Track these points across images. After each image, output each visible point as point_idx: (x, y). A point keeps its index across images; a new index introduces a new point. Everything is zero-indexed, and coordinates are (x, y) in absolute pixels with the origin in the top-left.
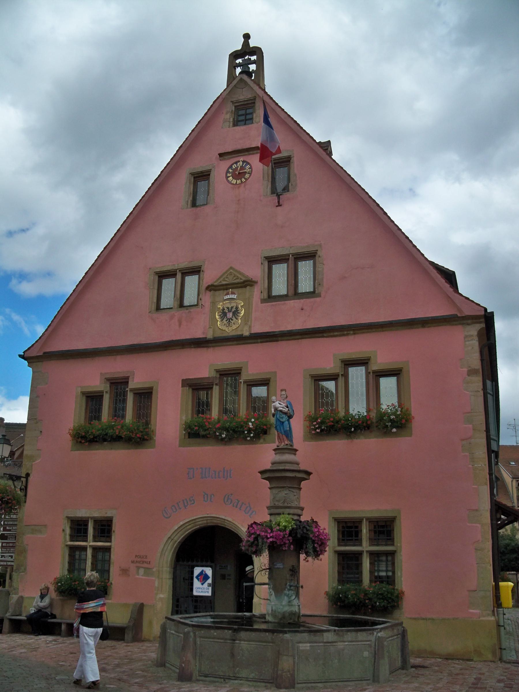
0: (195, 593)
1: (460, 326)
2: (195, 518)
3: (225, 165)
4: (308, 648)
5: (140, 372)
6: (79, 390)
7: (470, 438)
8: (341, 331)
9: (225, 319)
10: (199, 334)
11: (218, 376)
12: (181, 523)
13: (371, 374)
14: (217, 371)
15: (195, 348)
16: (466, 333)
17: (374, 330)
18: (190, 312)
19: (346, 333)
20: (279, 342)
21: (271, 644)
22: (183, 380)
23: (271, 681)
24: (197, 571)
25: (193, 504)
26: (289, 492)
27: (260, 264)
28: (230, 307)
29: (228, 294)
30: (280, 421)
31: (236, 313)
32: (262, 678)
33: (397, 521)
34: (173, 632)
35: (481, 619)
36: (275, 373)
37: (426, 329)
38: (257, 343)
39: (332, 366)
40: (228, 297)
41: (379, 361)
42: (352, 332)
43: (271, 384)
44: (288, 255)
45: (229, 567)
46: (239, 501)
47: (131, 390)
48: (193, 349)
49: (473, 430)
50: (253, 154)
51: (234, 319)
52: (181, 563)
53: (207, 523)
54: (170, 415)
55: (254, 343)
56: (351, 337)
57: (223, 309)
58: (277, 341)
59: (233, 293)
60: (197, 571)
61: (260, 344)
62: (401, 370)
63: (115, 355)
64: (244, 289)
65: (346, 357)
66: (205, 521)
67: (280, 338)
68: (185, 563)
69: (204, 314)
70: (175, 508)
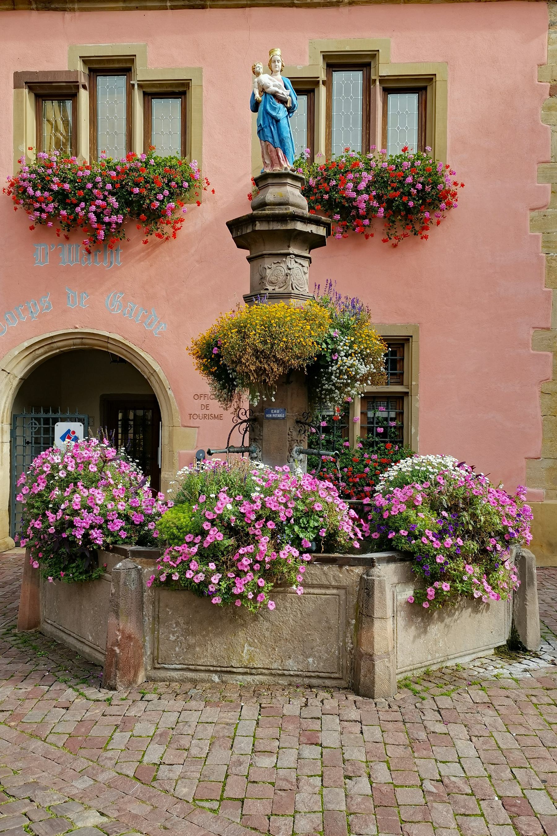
2: (51, 335)
13: (378, 83)
15: (38, 9)
22: (16, 74)
24: (61, 428)
33: (414, 344)
38: (165, 8)
39: (307, 62)
43: (194, 93)
48: (35, 14)
61: (170, 11)
66: (78, 341)
68: (33, 415)
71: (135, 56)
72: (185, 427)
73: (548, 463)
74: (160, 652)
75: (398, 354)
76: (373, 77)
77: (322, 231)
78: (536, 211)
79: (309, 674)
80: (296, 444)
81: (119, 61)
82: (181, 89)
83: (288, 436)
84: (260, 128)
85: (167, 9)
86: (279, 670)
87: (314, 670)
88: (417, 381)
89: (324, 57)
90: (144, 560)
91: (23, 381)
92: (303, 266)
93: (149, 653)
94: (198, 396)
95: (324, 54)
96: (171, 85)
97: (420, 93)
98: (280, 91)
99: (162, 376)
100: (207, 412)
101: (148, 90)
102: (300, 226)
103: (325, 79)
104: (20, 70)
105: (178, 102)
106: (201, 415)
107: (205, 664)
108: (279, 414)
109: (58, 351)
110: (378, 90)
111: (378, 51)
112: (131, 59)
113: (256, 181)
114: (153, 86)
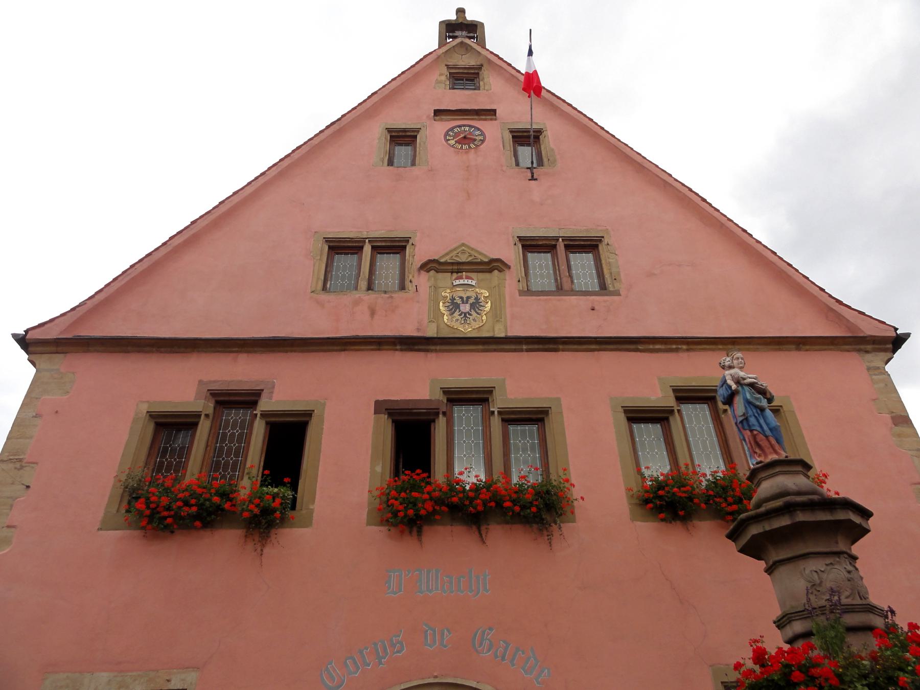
1: (855, 354)
3: (442, 126)
5: (286, 386)
6: (144, 408)
9: (457, 313)
10: (409, 331)
15: (401, 350)
18: (392, 297)
19: (674, 347)
25: (398, 652)
27: (513, 245)
28: (465, 297)
29: (461, 278)
30: (756, 407)
31: (476, 305)
36: (558, 399)
38: (522, 350)
39: (660, 394)
40: (462, 282)
42: (684, 347)
44: (556, 239)
47: (264, 415)
48: (398, 354)
50: (485, 120)
51: (473, 312)
54: (347, 464)
55: (515, 351)
57: (453, 299)
59: (467, 278)
63: (237, 352)
64: (487, 275)
67: (561, 347)
69: (418, 302)
70: (355, 663)
81: (478, 392)
89: (674, 391)
112: (490, 391)
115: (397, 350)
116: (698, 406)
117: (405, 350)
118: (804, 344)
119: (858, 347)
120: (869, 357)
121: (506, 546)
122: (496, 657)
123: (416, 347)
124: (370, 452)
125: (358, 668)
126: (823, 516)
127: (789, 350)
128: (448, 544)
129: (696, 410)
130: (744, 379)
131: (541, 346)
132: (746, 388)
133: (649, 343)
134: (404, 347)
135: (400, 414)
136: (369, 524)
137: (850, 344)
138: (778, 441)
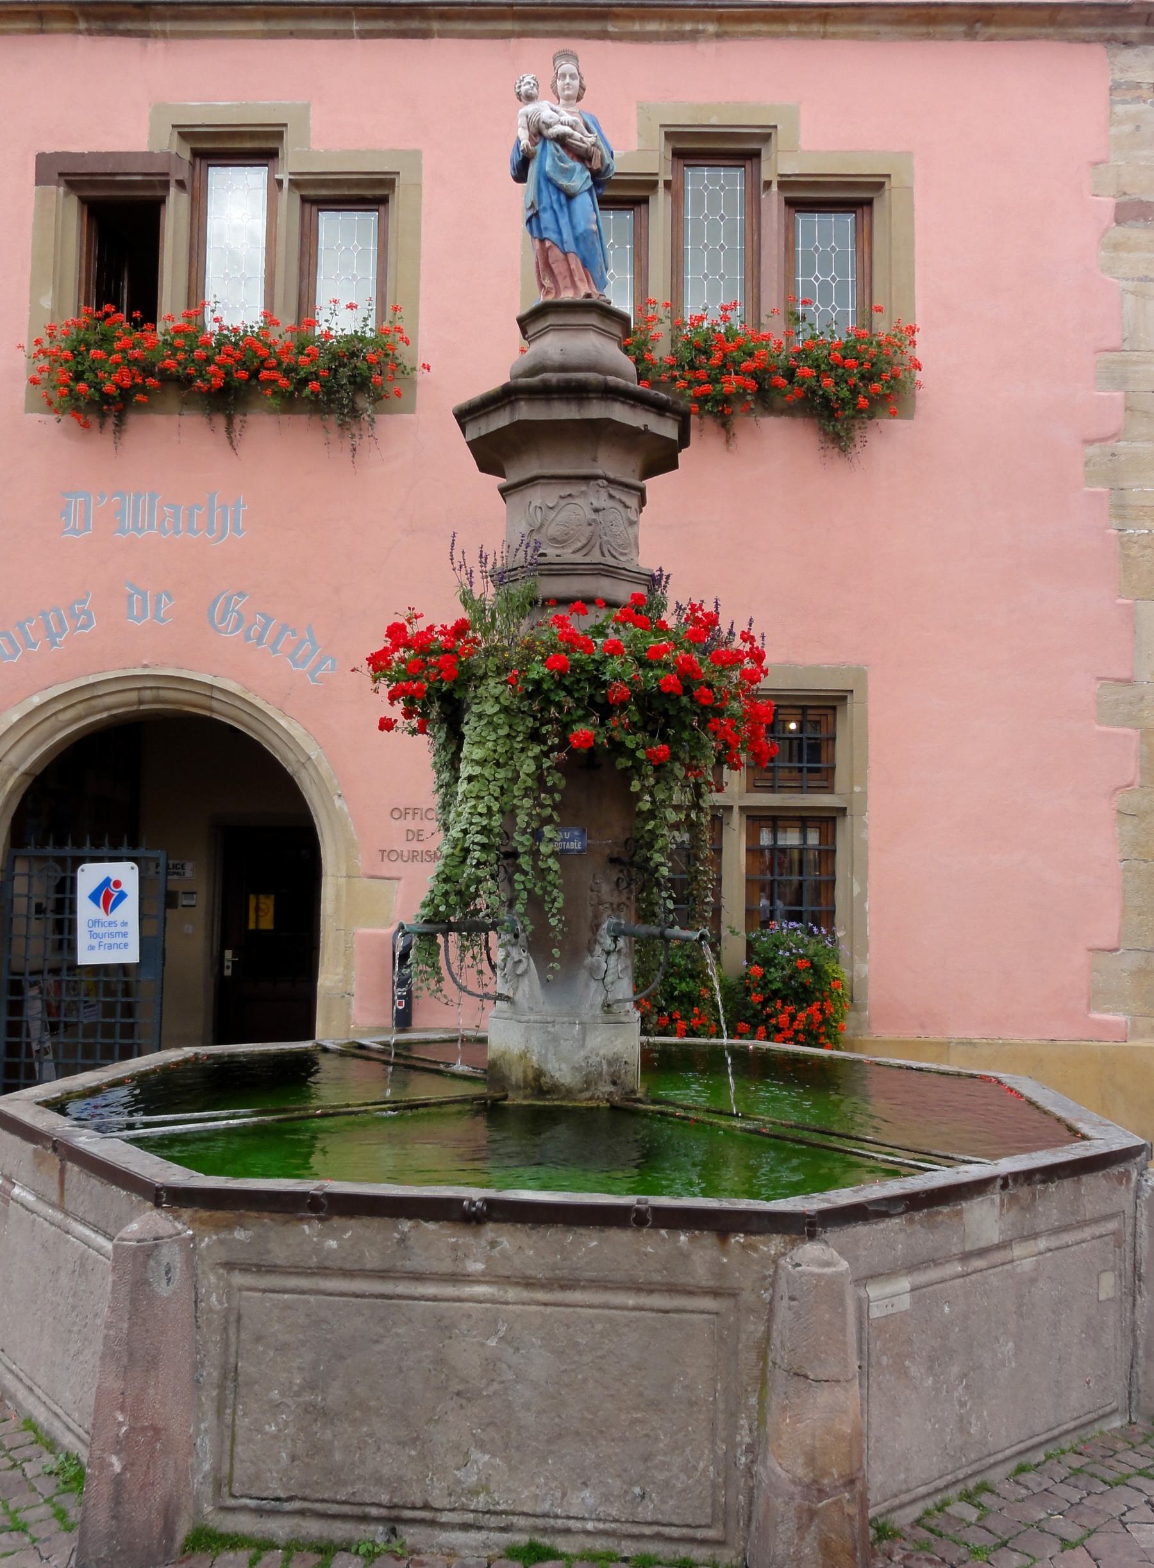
0: (86, 956)
1: (1098, 49)
4: (905, 1303)
7: (1115, 436)
8: (670, 18)
11: (187, 155)
12: (37, 700)
13: (774, 187)
14: (186, 134)
15: (90, 32)
16: (1118, 76)
17: (793, 28)
19: (688, 27)
20: (434, 43)
21: (708, 1303)
22: (42, 159)
23: (711, 1534)
24: (89, 876)
25: (83, 627)
26: (610, 503)
30: (559, 189)
32: (646, 1511)
34: (30, 1198)
35: (1130, 1043)
36: (417, 154)
37: (978, 45)
38: (348, 35)
39: (635, 145)
41: (806, 142)
42: (711, 28)
43: (400, 199)
45: (189, 866)
46: (269, 619)
48: (83, 42)
49: (1127, 409)
52: (31, 850)
53: (141, 702)
55: (335, 35)
56: (707, 49)
58: (425, 35)
60: (89, 876)
61: (358, 43)
62: (881, 185)
65: (684, 118)
66: (133, 696)
67: (436, 26)
68: (50, 850)
71: (285, 125)
72: (372, 877)
73: (1132, 961)
74: (237, 1466)
75: (824, 729)
76: (765, 177)
77: (668, 429)
78: (1097, 444)
79: (636, 1530)
80: (609, 912)
81: (253, 136)
82: (378, 192)
83: (590, 893)
84: (530, 213)
85: (353, 37)
86: (557, 1517)
87: (649, 1519)
88: (864, 784)
89: (669, 136)
90: (204, 1214)
91: (30, 781)
92: (626, 507)
93: (207, 1467)
94: (399, 813)
95: (667, 129)
96: (358, 183)
97: (859, 211)
98: (577, 135)
99: (325, 768)
100: (419, 847)
101: (311, 192)
102: (621, 413)
103: (670, 177)
104: (49, 148)
105: (373, 217)
106: (405, 853)
107: (357, 1499)
108: (569, 841)
109: (105, 715)
110: (773, 202)
111: (775, 127)
112: (277, 134)
113: (524, 322)
114: (323, 184)
115: (79, 32)
116: (722, 172)
117: (99, 32)
118: (988, 22)
119: (1109, 31)
120: (1128, 56)
121: (277, 454)
122: (248, 638)
123: (121, 26)
124: (29, 268)
125: (17, 650)
126: (563, 412)
127: (950, 38)
128: (171, 450)
129: (714, 181)
130: (549, 126)
131: (391, 25)
132: (550, 146)
133: (630, 18)
134: (95, 25)
135: (93, 184)
136: (29, 409)
137: (1091, 23)
138: (585, 265)
